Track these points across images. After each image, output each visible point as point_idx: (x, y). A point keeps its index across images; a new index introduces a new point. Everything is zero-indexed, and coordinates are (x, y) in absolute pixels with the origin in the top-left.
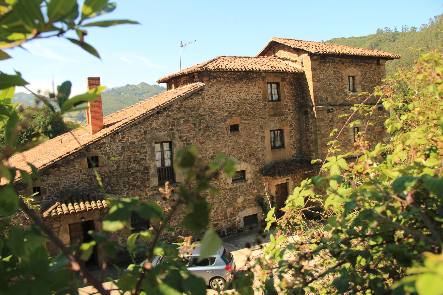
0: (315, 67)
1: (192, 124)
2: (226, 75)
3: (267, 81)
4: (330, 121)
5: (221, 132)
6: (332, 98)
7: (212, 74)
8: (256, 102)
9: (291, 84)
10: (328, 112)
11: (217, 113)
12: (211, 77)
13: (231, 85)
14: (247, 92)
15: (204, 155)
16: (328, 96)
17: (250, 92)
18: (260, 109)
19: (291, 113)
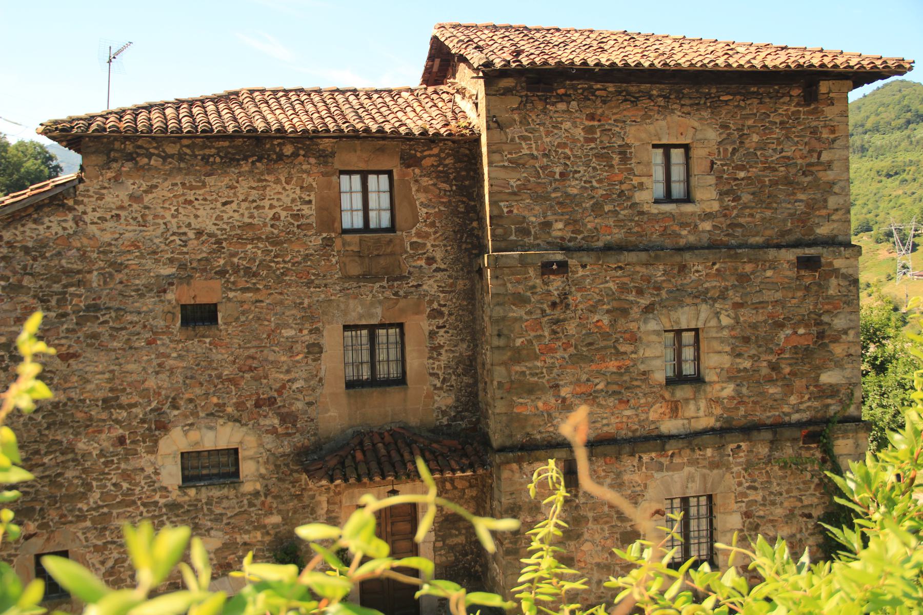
0: (504, 116)
1: (35, 297)
2: (171, 149)
3: (338, 166)
4: (554, 305)
5: (145, 326)
6: (572, 222)
7: (117, 145)
8: (288, 233)
9: (443, 176)
10: (543, 274)
11: (134, 267)
12: (112, 154)
13: (190, 180)
14: (254, 201)
15: (73, 395)
16: (551, 218)
17: (266, 203)
18: (307, 255)
19: (438, 270)
